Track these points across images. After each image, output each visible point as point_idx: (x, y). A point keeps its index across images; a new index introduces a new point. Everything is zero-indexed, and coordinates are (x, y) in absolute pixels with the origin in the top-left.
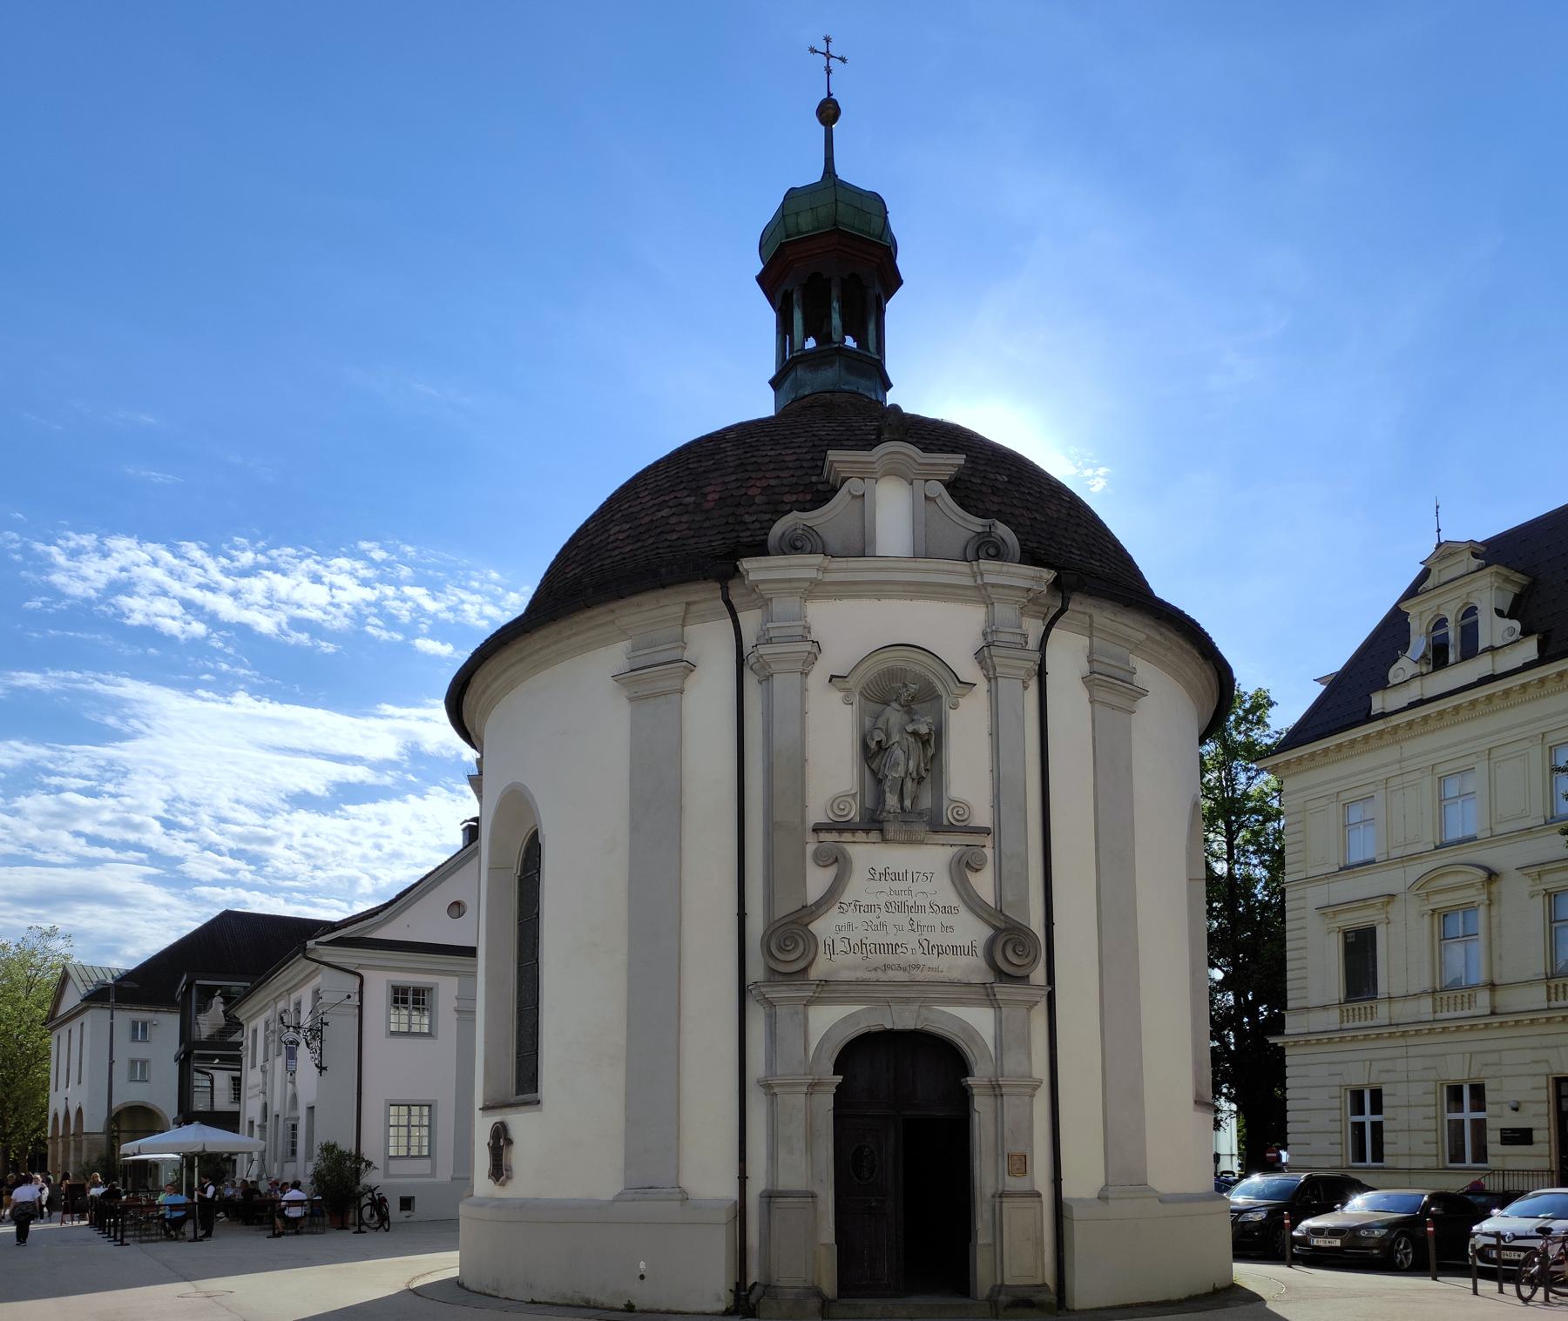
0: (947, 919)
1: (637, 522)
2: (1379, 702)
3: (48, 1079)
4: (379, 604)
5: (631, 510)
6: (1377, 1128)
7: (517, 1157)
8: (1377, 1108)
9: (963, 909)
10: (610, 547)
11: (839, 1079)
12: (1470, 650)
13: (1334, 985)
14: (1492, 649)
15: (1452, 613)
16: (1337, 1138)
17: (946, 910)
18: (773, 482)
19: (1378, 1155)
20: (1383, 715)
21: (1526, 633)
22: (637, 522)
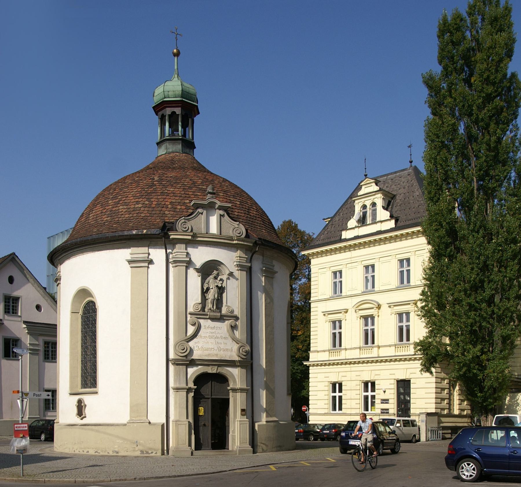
0: (225, 341)
1: (129, 207)
2: (345, 235)
3: (403, 420)
4: (360, 439)
5: (126, 201)
6: (340, 398)
7: (87, 411)
8: (373, 390)
9: (229, 338)
10: (120, 213)
11: (196, 387)
12: (374, 222)
13: (329, 292)
14: (381, 222)
15: (368, 203)
16: (326, 402)
17: (225, 338)
18: (174, 201)
19: (340, 409)
20: (346, 240)
21: (392, 217)
22: (129, 207)
